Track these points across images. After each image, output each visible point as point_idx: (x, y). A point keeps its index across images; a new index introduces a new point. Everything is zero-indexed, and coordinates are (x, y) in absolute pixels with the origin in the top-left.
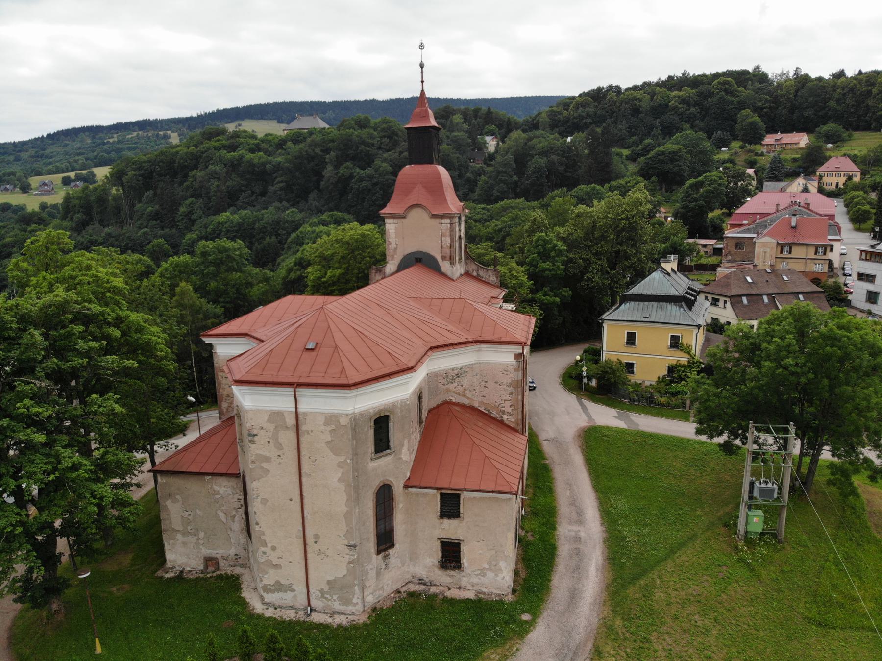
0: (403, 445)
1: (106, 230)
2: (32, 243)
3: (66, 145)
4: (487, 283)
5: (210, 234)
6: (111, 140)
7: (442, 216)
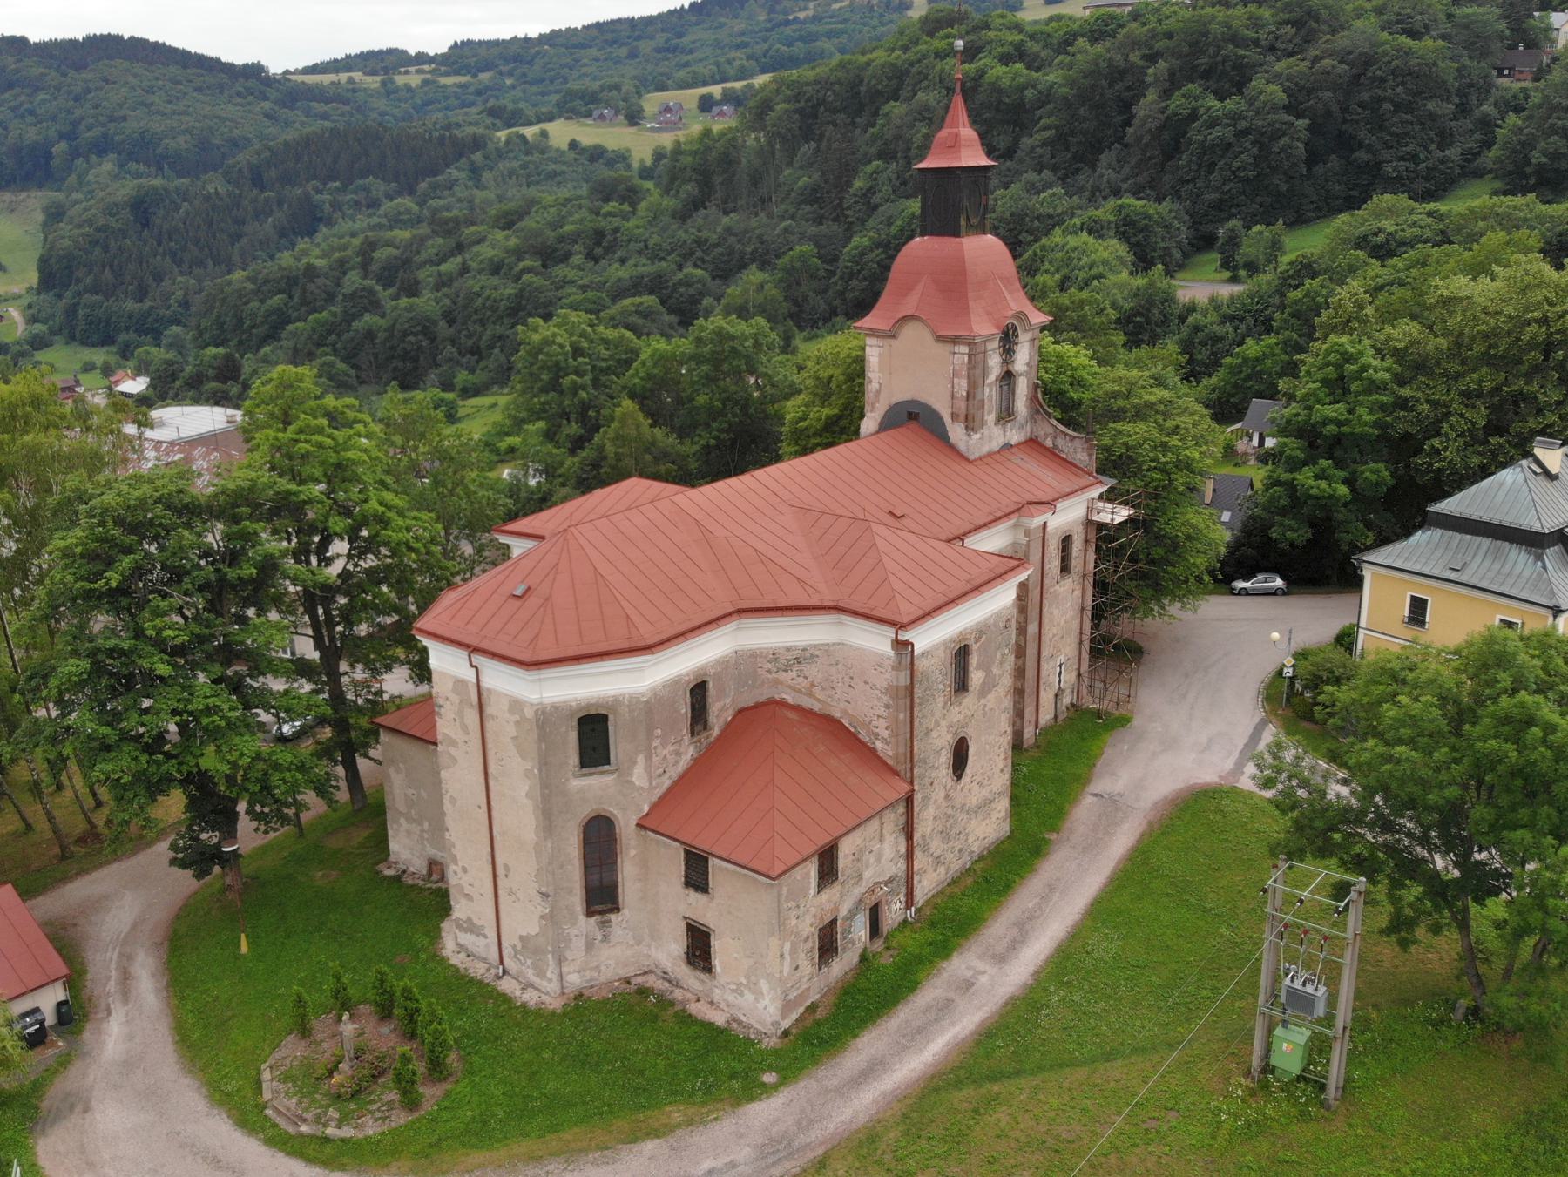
0: (635, 763)
1: (726, 220)
3: (721, 26)
4: (1069, 464)
5: (895, 237)
6: (802, 15)
7: (955, 340)
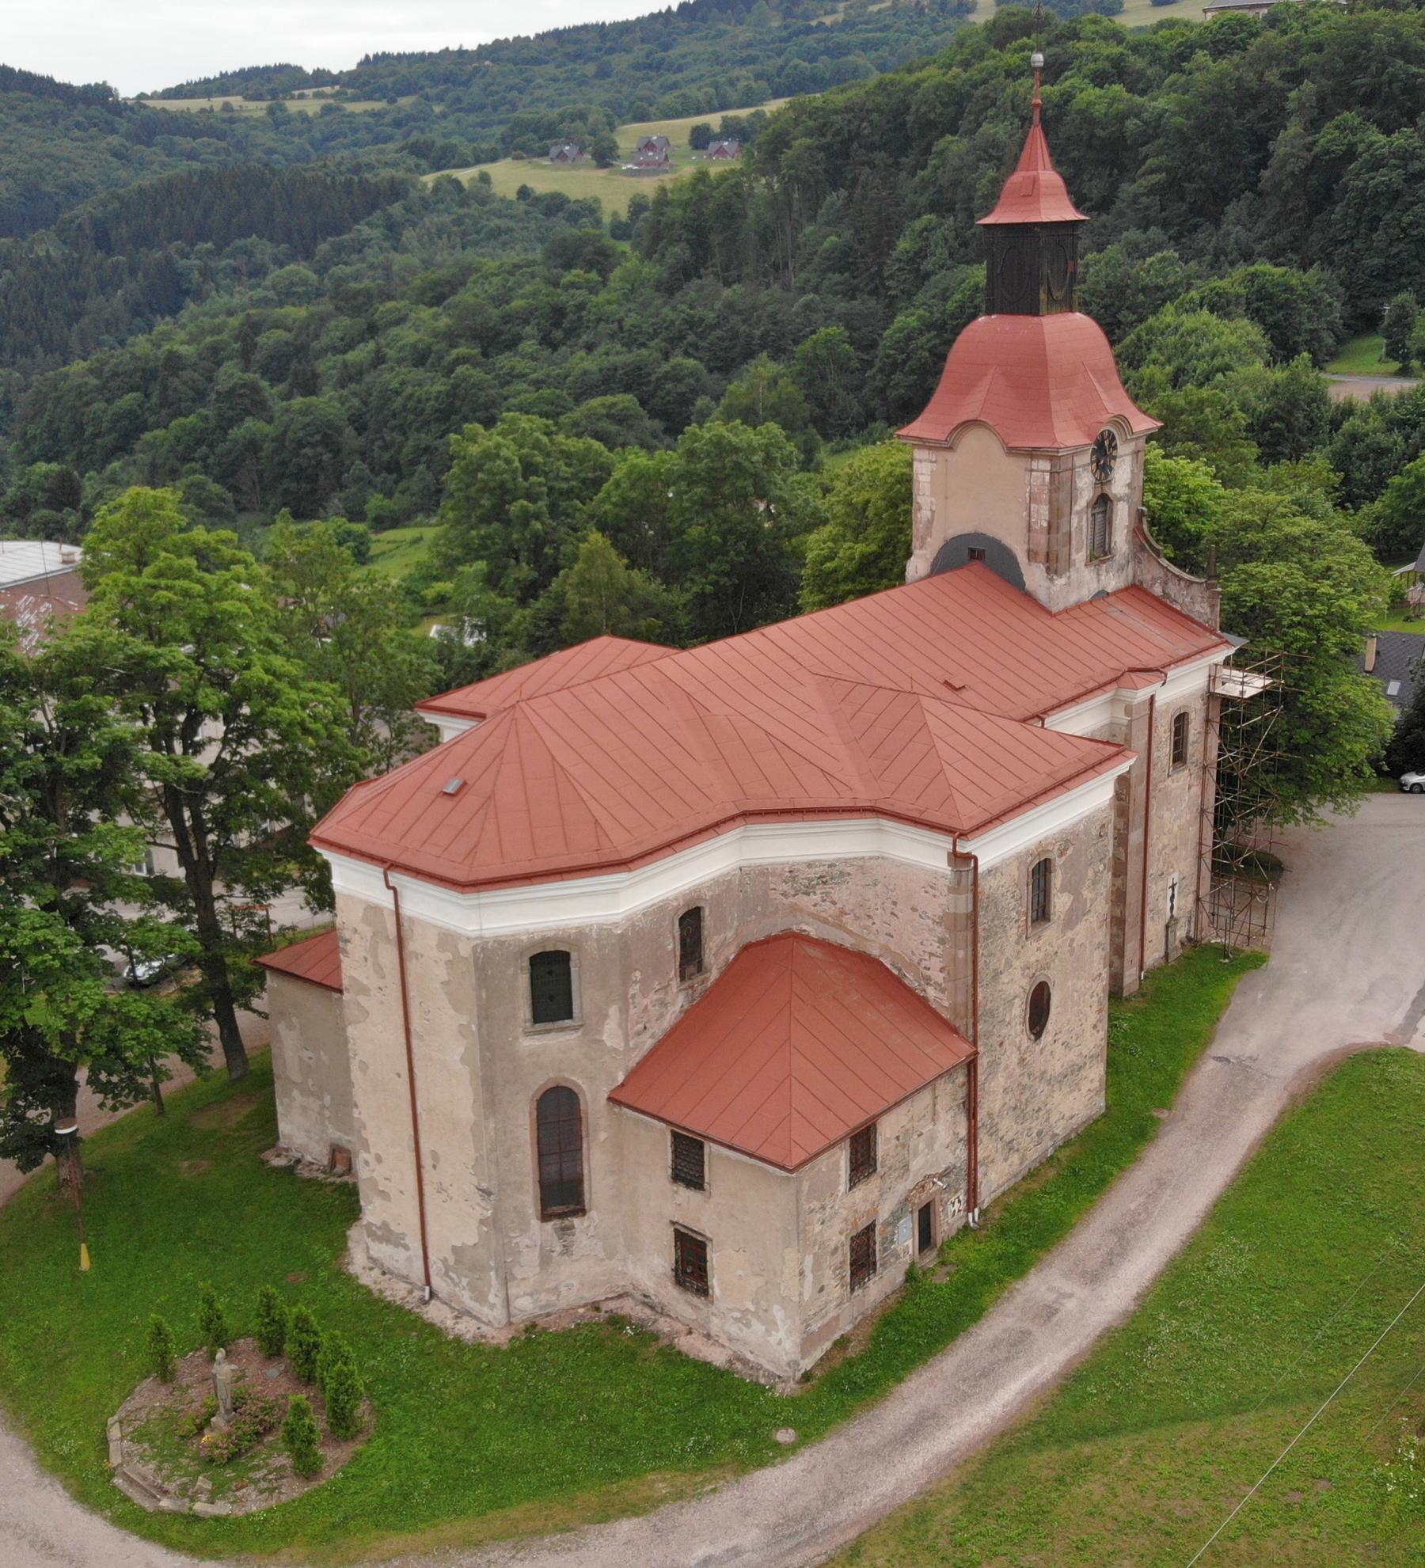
0: (606, 1016)
2: (110, 512)
3: (721, 34)
5: (953, 316)
6: (828, 20)
7: (1032, 453)
